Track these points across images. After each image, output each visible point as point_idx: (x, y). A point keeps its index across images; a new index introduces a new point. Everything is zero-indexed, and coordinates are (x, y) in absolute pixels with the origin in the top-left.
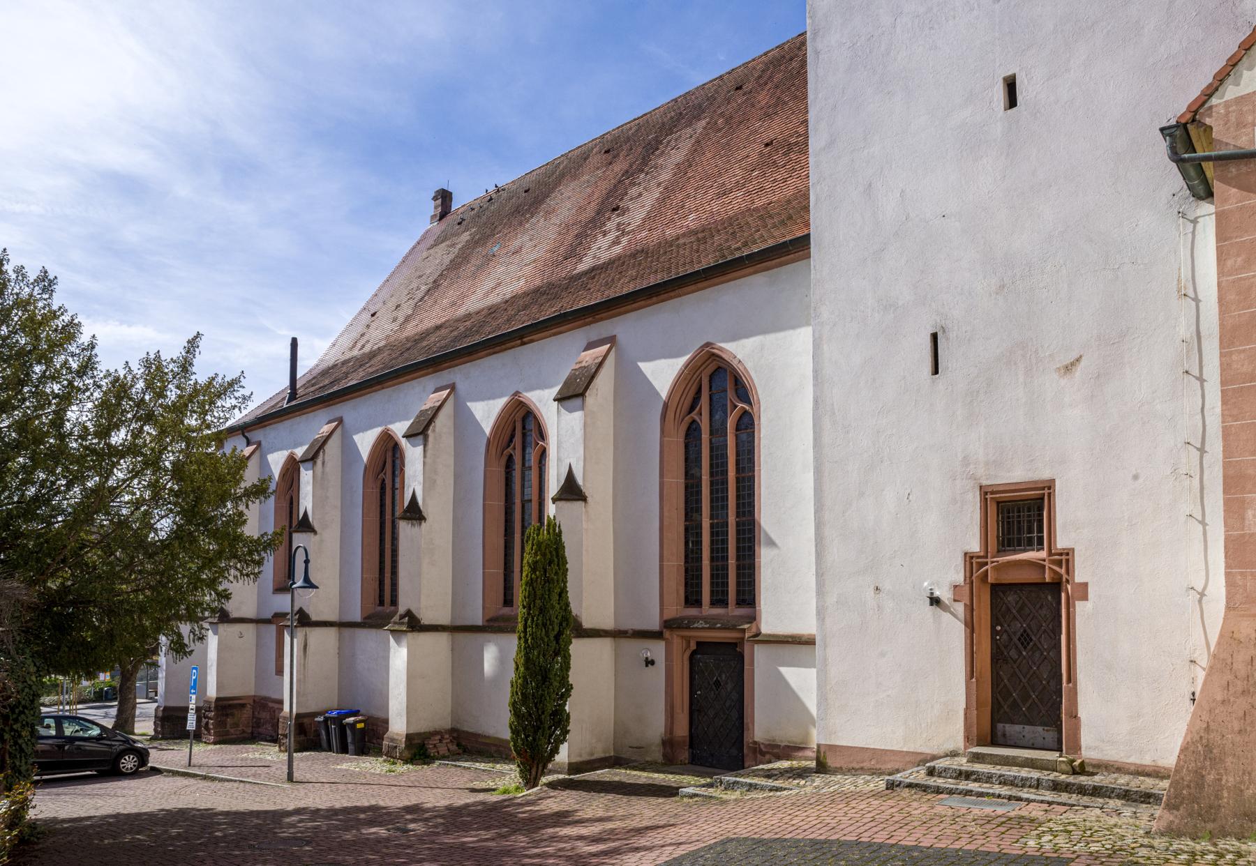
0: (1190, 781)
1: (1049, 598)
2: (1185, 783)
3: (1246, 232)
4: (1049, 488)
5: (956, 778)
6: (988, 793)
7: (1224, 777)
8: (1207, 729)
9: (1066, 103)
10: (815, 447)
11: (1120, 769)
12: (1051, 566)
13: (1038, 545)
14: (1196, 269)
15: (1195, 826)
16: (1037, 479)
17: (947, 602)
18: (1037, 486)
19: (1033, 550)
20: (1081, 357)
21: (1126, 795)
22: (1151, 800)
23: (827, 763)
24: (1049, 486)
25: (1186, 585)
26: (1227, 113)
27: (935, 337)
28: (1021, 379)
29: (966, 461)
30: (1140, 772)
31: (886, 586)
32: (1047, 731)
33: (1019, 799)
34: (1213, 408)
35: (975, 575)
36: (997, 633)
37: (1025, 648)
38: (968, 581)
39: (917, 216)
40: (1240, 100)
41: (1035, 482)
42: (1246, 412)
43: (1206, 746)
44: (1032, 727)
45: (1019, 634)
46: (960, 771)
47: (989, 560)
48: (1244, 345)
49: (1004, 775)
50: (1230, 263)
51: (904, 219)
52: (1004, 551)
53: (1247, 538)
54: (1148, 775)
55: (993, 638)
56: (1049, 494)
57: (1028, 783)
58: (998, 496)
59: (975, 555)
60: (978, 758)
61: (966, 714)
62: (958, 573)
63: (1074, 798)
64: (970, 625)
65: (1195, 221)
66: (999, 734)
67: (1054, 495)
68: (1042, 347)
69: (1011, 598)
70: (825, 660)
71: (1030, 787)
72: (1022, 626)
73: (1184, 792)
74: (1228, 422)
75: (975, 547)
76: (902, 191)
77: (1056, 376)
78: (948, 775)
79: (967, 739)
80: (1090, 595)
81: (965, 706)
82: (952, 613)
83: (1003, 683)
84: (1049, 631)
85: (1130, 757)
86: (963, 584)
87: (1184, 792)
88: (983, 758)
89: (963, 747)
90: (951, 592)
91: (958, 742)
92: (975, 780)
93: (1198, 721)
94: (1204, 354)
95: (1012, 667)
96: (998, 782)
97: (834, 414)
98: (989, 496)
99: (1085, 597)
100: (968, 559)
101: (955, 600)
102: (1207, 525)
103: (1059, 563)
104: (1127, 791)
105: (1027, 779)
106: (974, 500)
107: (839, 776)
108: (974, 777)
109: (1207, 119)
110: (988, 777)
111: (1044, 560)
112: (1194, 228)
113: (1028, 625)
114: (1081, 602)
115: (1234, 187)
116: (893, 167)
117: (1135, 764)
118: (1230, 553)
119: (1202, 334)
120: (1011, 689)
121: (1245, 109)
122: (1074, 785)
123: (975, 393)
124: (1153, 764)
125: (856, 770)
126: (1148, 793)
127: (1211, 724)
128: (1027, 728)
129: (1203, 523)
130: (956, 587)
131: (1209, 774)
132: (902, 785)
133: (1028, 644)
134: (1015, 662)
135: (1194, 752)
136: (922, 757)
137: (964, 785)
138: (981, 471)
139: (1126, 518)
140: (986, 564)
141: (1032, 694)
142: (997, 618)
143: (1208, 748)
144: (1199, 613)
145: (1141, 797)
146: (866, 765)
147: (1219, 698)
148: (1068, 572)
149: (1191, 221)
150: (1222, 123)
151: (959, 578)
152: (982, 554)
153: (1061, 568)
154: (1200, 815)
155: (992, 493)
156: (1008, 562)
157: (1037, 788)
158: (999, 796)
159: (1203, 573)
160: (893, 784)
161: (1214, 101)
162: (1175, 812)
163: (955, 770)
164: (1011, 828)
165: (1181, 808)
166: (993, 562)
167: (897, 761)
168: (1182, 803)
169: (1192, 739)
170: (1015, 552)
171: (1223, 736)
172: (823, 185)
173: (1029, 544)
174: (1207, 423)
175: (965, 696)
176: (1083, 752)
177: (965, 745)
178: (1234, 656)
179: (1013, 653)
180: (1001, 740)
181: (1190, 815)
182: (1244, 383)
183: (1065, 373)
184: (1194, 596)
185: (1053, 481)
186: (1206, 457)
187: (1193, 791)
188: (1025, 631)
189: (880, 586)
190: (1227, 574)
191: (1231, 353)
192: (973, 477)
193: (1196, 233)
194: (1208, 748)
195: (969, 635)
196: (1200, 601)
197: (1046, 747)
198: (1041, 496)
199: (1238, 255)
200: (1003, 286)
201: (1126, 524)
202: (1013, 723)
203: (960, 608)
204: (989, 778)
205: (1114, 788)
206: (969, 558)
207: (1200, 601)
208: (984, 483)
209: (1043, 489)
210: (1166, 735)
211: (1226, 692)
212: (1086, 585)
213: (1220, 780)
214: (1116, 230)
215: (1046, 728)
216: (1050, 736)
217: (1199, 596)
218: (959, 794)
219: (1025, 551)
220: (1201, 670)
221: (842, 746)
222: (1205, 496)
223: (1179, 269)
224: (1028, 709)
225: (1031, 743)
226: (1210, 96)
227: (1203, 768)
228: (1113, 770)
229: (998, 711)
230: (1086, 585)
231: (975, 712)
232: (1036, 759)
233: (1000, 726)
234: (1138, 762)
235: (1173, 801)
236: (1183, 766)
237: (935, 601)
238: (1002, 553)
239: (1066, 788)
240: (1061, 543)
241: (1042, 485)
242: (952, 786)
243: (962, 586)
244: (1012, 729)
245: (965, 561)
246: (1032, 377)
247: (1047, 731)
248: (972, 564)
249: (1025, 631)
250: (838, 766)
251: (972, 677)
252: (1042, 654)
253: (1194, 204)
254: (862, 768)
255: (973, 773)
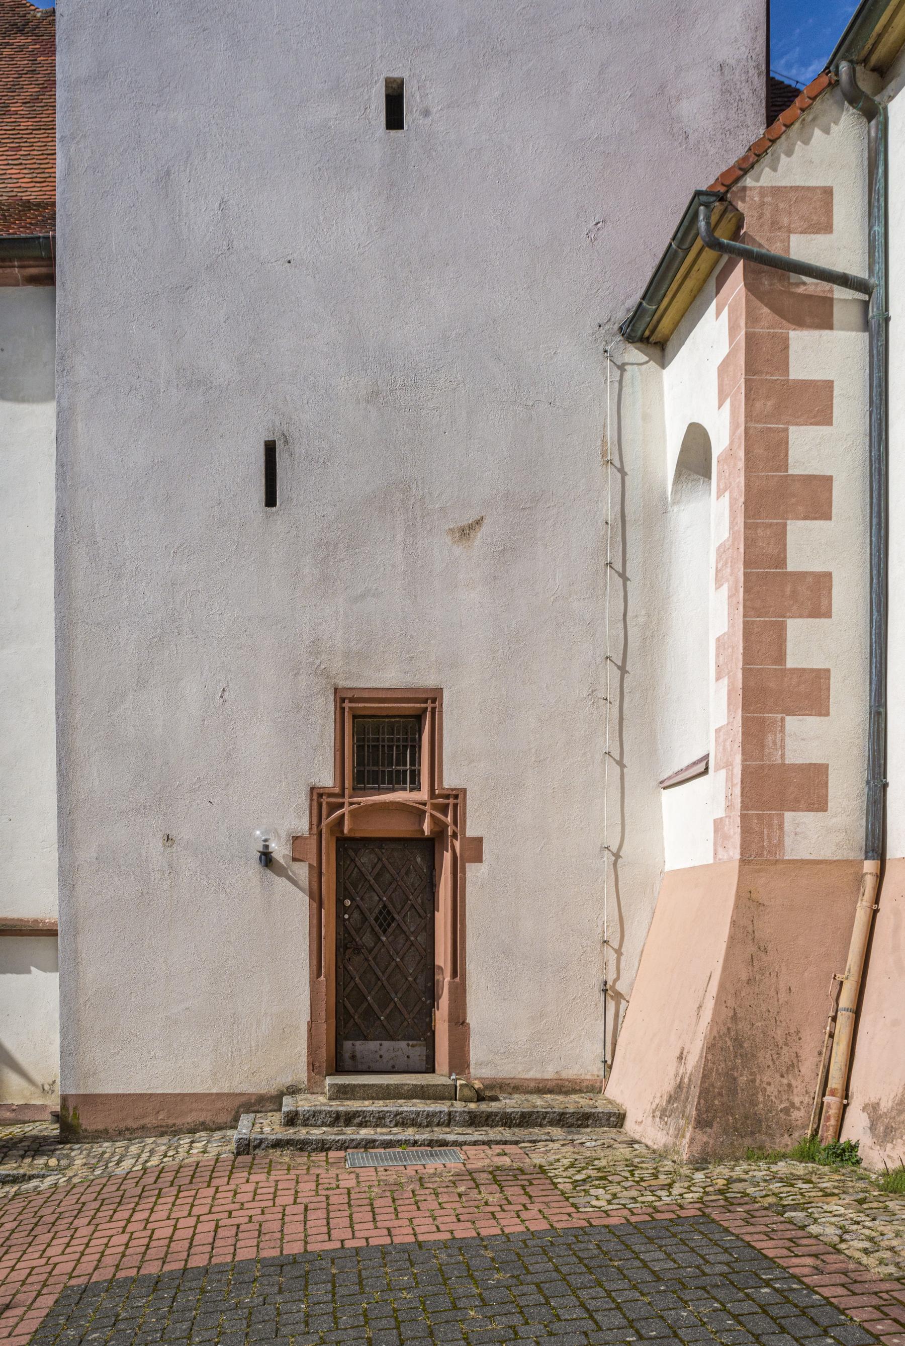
0: (722, 1088)
1: (419, 860)
2: (716, 1090)
3: (777, 369)
4: (434, 701)
5: (332, 1125)
6: (398, 1141)
7: (758, 1077)
8: (735, 1018)
9: (472, 150)
10: (58, 593)
11: (515, 1087)
12: (434, 813)
13: (411, 783)
14: (623, 432)
15: (732, 1144)
16: (418, 686)
17: (282, 861)
18: (417, 696)
19: (405, 789)
20: (482, 519)
21: (561, 1120)
22: (590, 1122)
23: (80, 1125)
24: (434, 697)
25: (599, 844)
26: (763, 204)
27: (270, 449)
28: (400, 537)
29: (316, 649)
30: (542, 1089)
31: (183, 833)
32: (413, 1046)
33: (444, 1144)
34: (636, 616)
35: (325, 822)
36: (346, 910)
37: (384, 932)
38: (315, 830)
39: (246, 248)
40: (777, 191)
41: (415, 690)
42: (771, 607)
43: (735, 1040)
44: (393, 1043)
45: (377, 911)
46: (337, 1113)
47: (346, 800)
48: (771, 519)
49: (402, 1113)
50: (758, 405)
51: (225, 247)
52: (364, 789)
53: (766, 771)
54: (550, 1092)
55: (338, 917)
56: (352, 700)
57: (436, 1120)
58: (360, 705)
59: (326, 791)
60: (345, 1093)
61: (310, 1030)
62: (300, 818)
63: (506, 1134)
64: (317, 897)
65: (622, 368)
66: (347, 1055)
67: (441, 711)
68: (430, 494)
69: (365, 859)
70: (76, 953)
71: (438, 1125)
72: (381, 899)
73: (716, 1102)
74: (750, 616)
75: (327, 779)
76: (223, 202)
77: (448, 540)
78: (319, 1122)
79: (312, 1066)
80: (485, 856)
81: (308, 1019)
82: (290, 879)
83: (352, 984)
84: (418, 907)
85: (530, 1070)
86: (307, 834)
87: (716, 1102)
88: (353, 1091)
89: (305, 1080)
90: (289, 847)
91: (300, 1073)
92: (360, 1125)
93: (724, 1007)
94: (628, 545)
95: (366, 959)
96: (393, 1124)
97: (95, 542)
98: (347, 705)
99: (478, 859)
100: (315, 797)
101: (294, 859)
102: (625, 766)
103: (444, 809)
104: (563, 1114)
105: (434, 1114)
106: (326, 707)
107: (106, 1144)
108: (357, 1120)
109: (740, 203)
110: (379, 1118)
111: (425, 804)
112: (622, 376)
113: (390, 898)
114: (473, 865)
115: (766, 305)
116: (209, 156)
117: (536, 1079)
118: (747, 789)
119: (627, 519)
120: (365, 991)
121: (781, 205)
122: (496, 1114)
123: (332, 546)
124: (556, 1077)
125: (132, 1131)
126: (587, 1113)
127: (738, 1010)
128: (386, 1044)
129: (621, 764)
130: (295, 838)
131: (741, 1075)
132: (263, 1146)
133: (389, 925)
134: (370, 951)
135: (722, 1049)
136: (243, 1099)
137: (350, 1133)
138: (337, 666)
139: (533, 751)
140: (342, 805)
141: (393, 995)
142: (346, 889)
143: (738, 1042)
144: (614, 880)
145: (578, 1120)
146: (150, 1121)
147: (744, 976)
148: (455, 822)
149: (619, 367)
150: (756, 214)
151: (302, 825)
152: (337, 790)
153: (447, 816)
154: (736, 1129)
155: (352, 700)
156: (371, 805)
157: (448, 1125)
158: (415, 1143)
159: (619, 828)
160: (248, 1145)
161: (749, 181)
162: (708, 1130)
163: (330, 1112)
164: (30, 1202)
165: (715, 1124)
166: (351, 804)
167: (201, 1110)
168: (715, 1117)
169: (719, 1032)
170: (380, 791)
171: (753, 1025)
172: (82, 145)
173: (397, 781)
174: (629, 634)
175: (308, 1004)
176: (472, 1071)
177: (309, 1076)
178: (755, 922)
179: (367, 939)
180: (348, 1064)
181: (725, 1131)
182: (769, 568)
183: (461, 538)
184: (608, 858)
185: (440, 691)
186: (628, 679)
187: (725, 1099)
188: (385, 907)
189: (173, 834)
190: (743, 817)
191: (757, 526)
192: (325, 674)
193: (624, 383)
194: (738, 1042)
195: (315, 911)
196: (615, 864)
197: (410, 1070)
198: (418, 713)
199: (768, 397)
200: (378, 393)
201: (533, 759)
202: (366, 1038)
203: (302, 871)
204: (379, 1120)
205: (547, 1113)
206: (317, 794)
207: (615, 864)
208: (342, 684)
209: (425, 701)
210: (572, 1038)
211: (750, 968)
212: (480, 840)
213: (754, 1081)
214: (530, 353)
215: (411, 1043)
216: (417, 1052)
217: (614, 858)
218: (356, 1147)
219: (393, 790)
220: (613, 952)
221: (107, 1095)
222: (624, 729)
223: (605, 426)
224: (388, 1017)
225: (390, 1064)
226: (746, 172)
227: (734, 1068)
228: (510, 1090)
229: (346, 1024)
230: (480, 840)
231: (325, 1026)
232: (428, 1085)
233: (348, 1045)
234: (539, 1076)
235: (704, 1116)
236: (712, 1069)
237: (267, 859)
238: (361, 792)
239: (487, 1120)
240: (450, 780)
241: (424, 696)
242: (333, 1137)
243: (306, 838)
244: (366, 1048)
245: (311, 800)
246: (415, 536)
247: (413, 1046)
248: (320, 805)
249: (385, 907)
250: (100, 1127)
251: (319, 974)
252: (408, 939)
253: (622, 345)
254: (143, 1128)
255: (356, 1114)
